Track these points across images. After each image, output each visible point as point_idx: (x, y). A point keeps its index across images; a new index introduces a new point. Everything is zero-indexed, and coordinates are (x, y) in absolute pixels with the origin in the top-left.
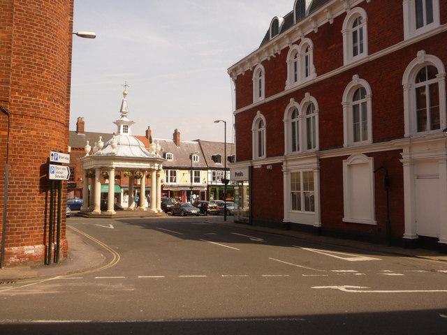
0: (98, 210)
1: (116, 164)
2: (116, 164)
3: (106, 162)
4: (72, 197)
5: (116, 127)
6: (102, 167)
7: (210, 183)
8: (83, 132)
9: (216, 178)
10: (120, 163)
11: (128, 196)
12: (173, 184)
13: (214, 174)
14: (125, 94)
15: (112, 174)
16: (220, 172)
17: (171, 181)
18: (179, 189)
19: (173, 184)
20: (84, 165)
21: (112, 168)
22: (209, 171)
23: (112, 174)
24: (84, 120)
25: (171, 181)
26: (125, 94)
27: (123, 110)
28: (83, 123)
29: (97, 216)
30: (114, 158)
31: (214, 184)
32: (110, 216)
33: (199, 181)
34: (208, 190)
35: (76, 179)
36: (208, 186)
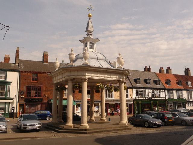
0: (70, 124)
1: (89, 76)
2: (89, 76)
3: (80, 73)
4: (40, 109)
5: (82, 46)
6: (74, 79)
7: (134, 98)
8: (47, 62)
9: (155, 95)
10: (93, 75)
11: (79, 108)
12: (110, 98)
13: (137, 91)
14: (90, 16)
15: (85, 85)
16: (140, 90)
17: (109, 97)
18: (115, 102)
19: (110, 98)
20: (54, 79)
21: (85, 79)
22: (134, 89)
23: (85, 85)
24: (48, 53)
25: (109, 97)
26: (90, 16)
27: (89, 29)
28: (47, 56)
29: (69, 131)
30: (87, 68)
31: (137, 98)
32: (84, 131)
33: (112, 97)
34: (133, 103)
35: (43, 95)
36: (134, 100)
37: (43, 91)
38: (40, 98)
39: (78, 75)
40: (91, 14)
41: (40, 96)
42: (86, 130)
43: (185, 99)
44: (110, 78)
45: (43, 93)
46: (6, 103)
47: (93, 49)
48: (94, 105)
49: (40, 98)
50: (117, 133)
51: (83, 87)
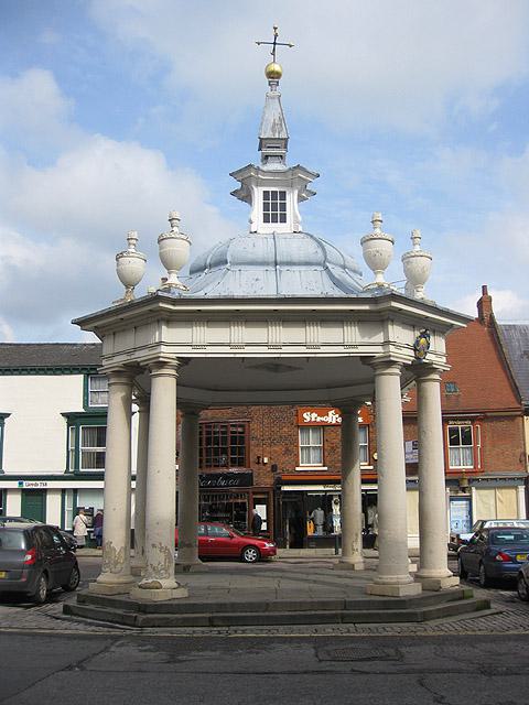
1: (176, 341)
2: (176, 341)
3: (141, 338)
21: (162, 365)
35: (253, 459)
37: (252, 442)
38: (243, 470)
39: (135, 350)
40: (276, 68)
41: (241, 463)
42: (402, 603)
43: (477, 488)
44: (303, 349)
45: (254, 452)
46: (63, 491)
47: (283, 220)
48: (33, 524)
49: (243, 470)
50: (456, 659)
51: (424, 416)
